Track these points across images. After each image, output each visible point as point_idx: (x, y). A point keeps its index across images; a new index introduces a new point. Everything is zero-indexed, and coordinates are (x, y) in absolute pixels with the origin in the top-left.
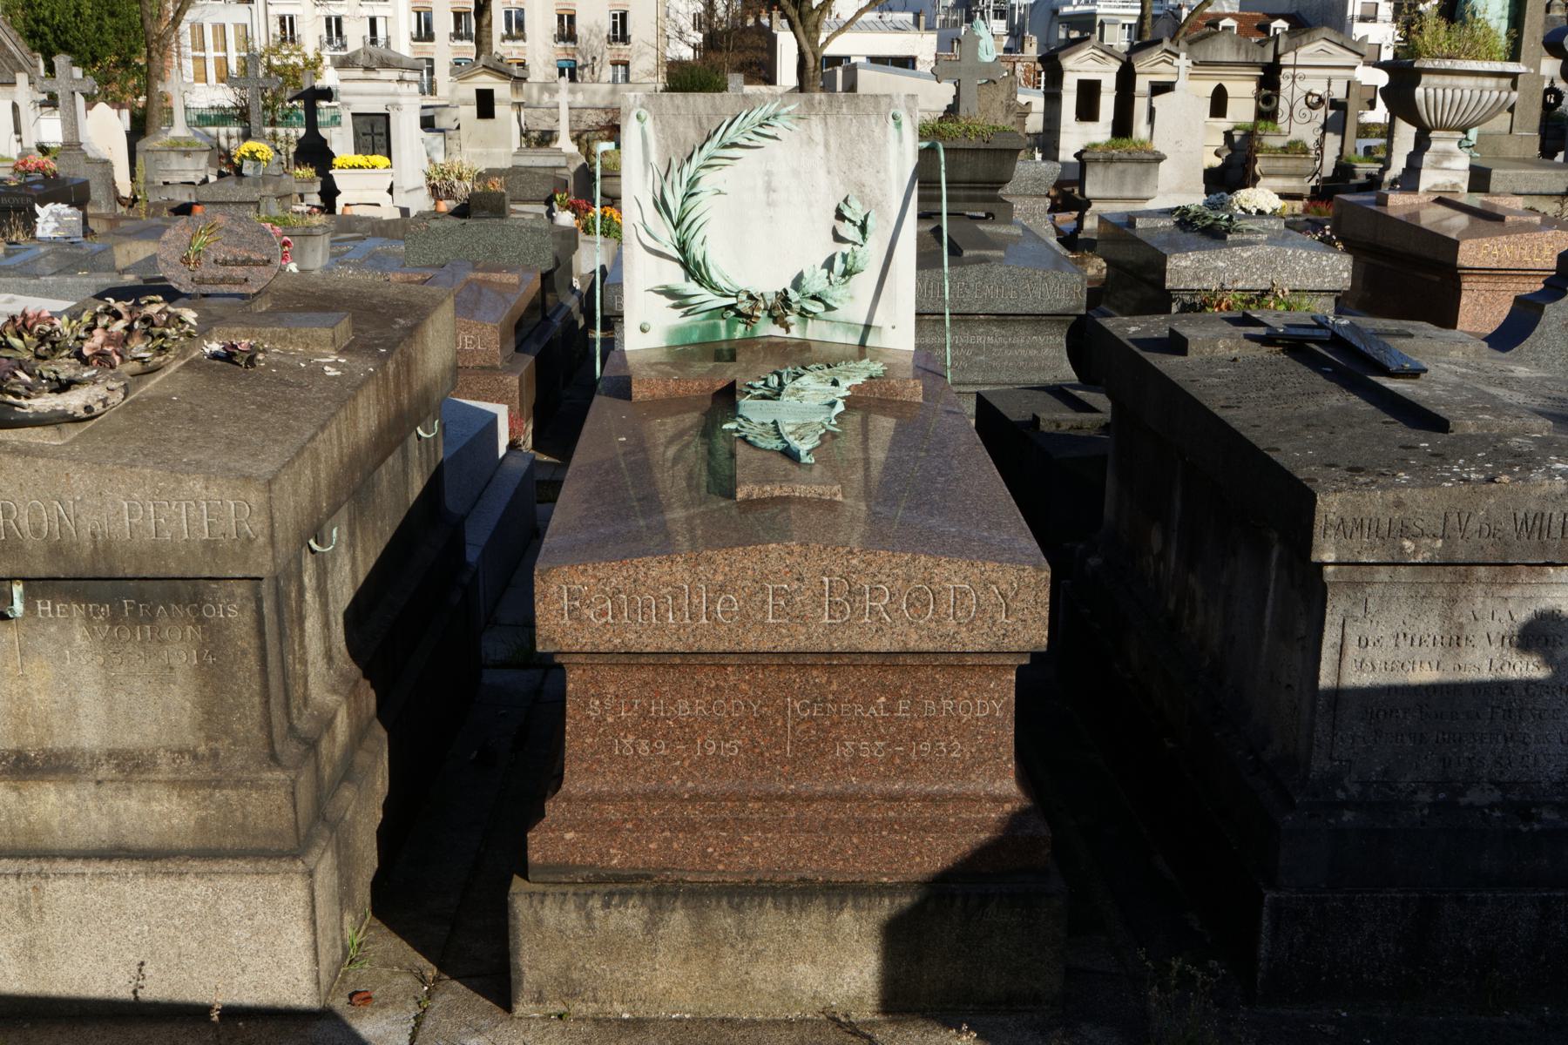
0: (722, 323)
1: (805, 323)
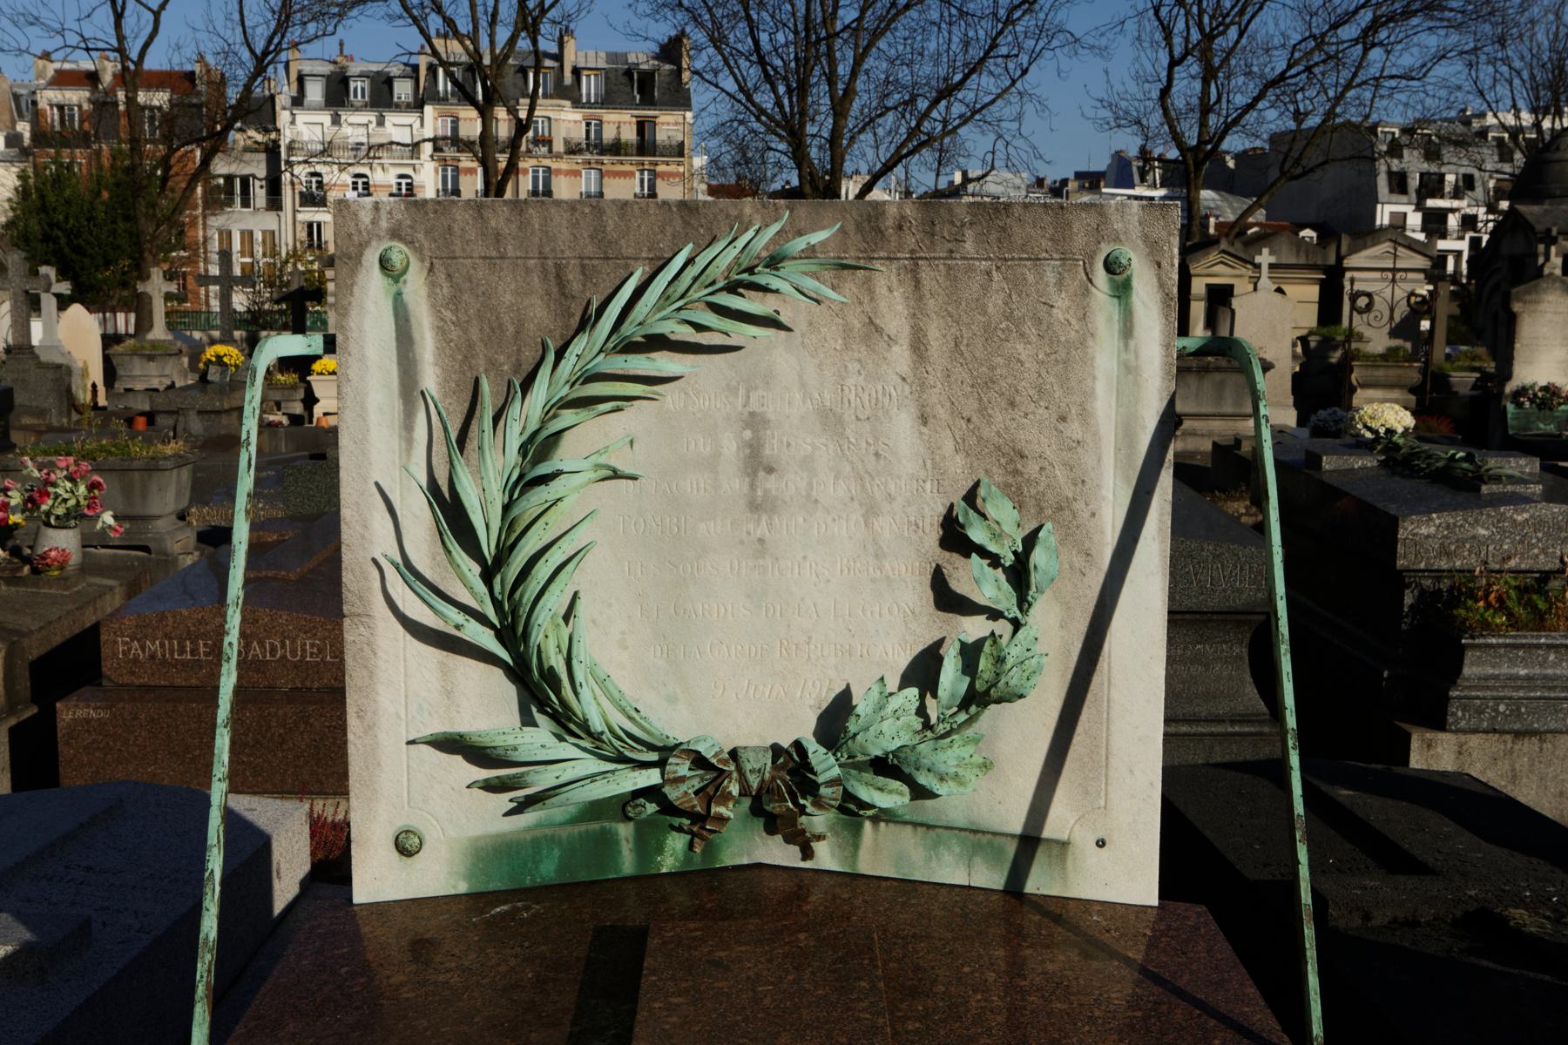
0: (625, 831)
1: (856, 830)
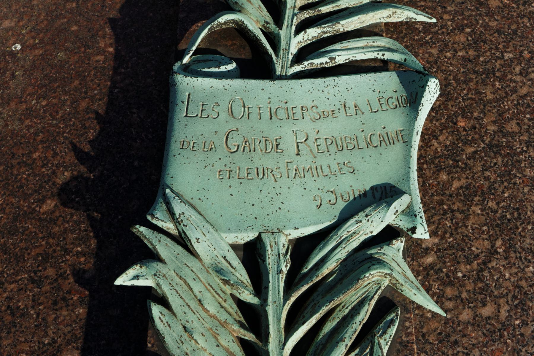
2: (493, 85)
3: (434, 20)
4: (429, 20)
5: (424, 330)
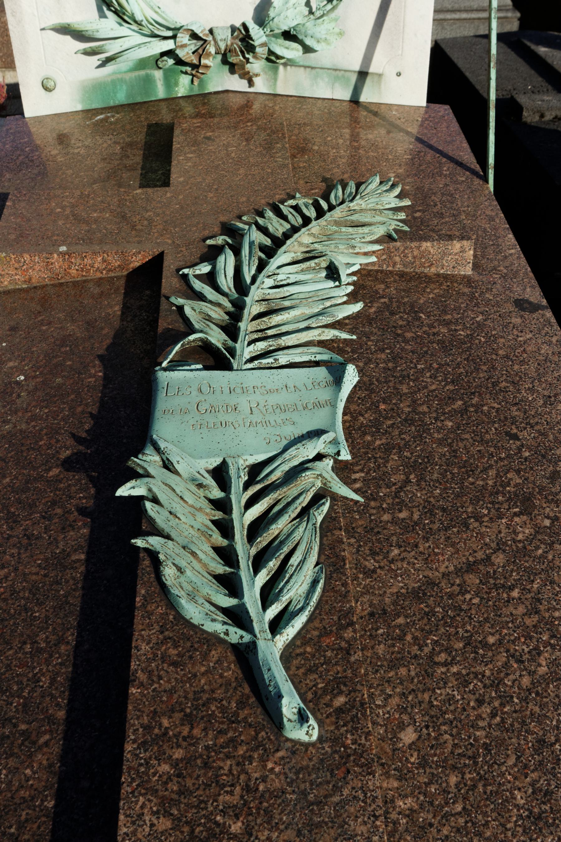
0: (158, 75)
1: (276, 70)
2: (408, 384)
3: (354, 337)
4: (350, 337)
5: (354, 525)
